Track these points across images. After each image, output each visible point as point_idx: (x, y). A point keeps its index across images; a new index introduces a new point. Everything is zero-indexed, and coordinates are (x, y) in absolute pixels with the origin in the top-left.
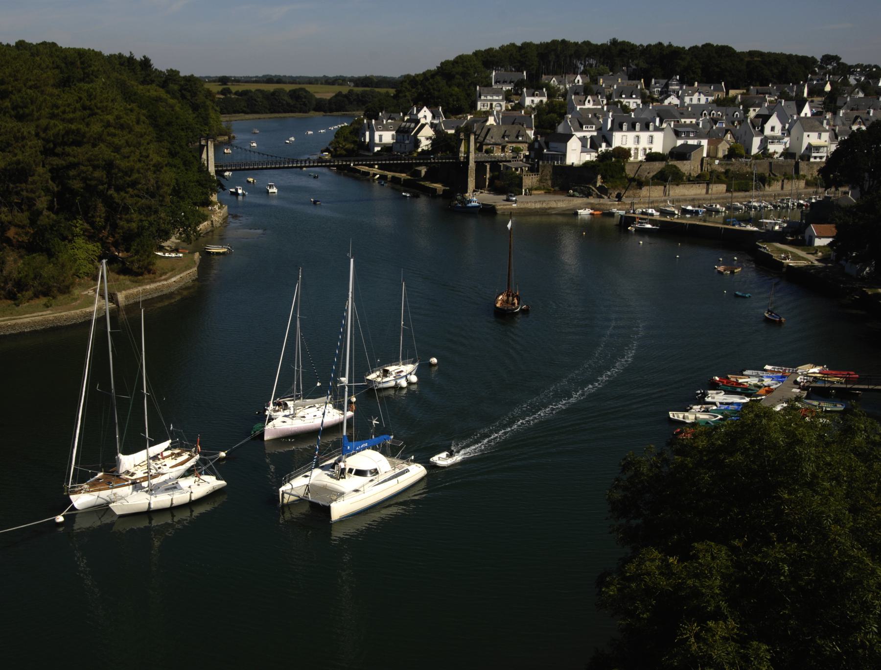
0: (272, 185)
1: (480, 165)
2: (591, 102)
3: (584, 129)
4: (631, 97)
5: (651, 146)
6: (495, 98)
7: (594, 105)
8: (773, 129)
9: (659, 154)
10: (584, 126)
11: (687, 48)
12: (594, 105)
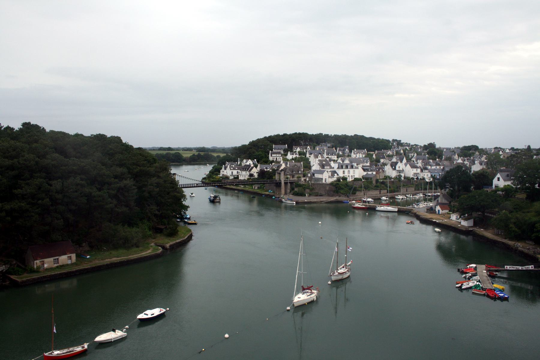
1: (286, 183)
2: (321, 157)
3: (325, 168)
4: (333, 155)
5: (354, 175)
6: (278, 155)
7: (322, 158)
8: (399, 167)
9: (357, 178)
10: (325, 167)
11: (333, 135)
12: (322, 158)
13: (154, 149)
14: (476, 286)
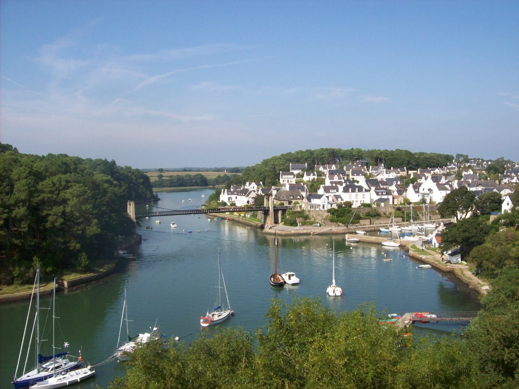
0: (294, 274)
2: (337, 178)
3: (331, 192)
10: (331, 190)
13: (179, 170)
14: (170, 338)
